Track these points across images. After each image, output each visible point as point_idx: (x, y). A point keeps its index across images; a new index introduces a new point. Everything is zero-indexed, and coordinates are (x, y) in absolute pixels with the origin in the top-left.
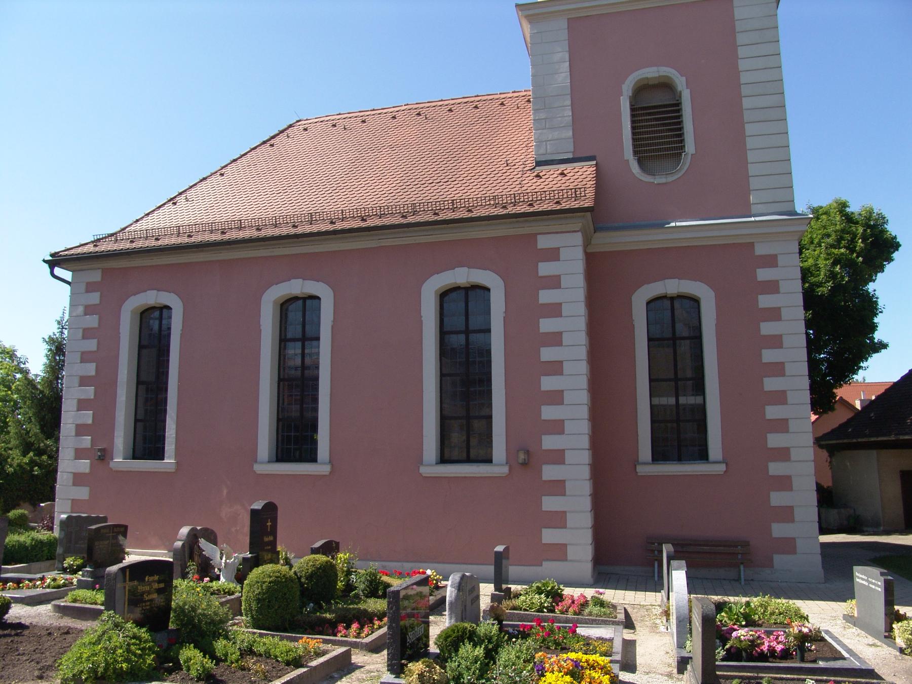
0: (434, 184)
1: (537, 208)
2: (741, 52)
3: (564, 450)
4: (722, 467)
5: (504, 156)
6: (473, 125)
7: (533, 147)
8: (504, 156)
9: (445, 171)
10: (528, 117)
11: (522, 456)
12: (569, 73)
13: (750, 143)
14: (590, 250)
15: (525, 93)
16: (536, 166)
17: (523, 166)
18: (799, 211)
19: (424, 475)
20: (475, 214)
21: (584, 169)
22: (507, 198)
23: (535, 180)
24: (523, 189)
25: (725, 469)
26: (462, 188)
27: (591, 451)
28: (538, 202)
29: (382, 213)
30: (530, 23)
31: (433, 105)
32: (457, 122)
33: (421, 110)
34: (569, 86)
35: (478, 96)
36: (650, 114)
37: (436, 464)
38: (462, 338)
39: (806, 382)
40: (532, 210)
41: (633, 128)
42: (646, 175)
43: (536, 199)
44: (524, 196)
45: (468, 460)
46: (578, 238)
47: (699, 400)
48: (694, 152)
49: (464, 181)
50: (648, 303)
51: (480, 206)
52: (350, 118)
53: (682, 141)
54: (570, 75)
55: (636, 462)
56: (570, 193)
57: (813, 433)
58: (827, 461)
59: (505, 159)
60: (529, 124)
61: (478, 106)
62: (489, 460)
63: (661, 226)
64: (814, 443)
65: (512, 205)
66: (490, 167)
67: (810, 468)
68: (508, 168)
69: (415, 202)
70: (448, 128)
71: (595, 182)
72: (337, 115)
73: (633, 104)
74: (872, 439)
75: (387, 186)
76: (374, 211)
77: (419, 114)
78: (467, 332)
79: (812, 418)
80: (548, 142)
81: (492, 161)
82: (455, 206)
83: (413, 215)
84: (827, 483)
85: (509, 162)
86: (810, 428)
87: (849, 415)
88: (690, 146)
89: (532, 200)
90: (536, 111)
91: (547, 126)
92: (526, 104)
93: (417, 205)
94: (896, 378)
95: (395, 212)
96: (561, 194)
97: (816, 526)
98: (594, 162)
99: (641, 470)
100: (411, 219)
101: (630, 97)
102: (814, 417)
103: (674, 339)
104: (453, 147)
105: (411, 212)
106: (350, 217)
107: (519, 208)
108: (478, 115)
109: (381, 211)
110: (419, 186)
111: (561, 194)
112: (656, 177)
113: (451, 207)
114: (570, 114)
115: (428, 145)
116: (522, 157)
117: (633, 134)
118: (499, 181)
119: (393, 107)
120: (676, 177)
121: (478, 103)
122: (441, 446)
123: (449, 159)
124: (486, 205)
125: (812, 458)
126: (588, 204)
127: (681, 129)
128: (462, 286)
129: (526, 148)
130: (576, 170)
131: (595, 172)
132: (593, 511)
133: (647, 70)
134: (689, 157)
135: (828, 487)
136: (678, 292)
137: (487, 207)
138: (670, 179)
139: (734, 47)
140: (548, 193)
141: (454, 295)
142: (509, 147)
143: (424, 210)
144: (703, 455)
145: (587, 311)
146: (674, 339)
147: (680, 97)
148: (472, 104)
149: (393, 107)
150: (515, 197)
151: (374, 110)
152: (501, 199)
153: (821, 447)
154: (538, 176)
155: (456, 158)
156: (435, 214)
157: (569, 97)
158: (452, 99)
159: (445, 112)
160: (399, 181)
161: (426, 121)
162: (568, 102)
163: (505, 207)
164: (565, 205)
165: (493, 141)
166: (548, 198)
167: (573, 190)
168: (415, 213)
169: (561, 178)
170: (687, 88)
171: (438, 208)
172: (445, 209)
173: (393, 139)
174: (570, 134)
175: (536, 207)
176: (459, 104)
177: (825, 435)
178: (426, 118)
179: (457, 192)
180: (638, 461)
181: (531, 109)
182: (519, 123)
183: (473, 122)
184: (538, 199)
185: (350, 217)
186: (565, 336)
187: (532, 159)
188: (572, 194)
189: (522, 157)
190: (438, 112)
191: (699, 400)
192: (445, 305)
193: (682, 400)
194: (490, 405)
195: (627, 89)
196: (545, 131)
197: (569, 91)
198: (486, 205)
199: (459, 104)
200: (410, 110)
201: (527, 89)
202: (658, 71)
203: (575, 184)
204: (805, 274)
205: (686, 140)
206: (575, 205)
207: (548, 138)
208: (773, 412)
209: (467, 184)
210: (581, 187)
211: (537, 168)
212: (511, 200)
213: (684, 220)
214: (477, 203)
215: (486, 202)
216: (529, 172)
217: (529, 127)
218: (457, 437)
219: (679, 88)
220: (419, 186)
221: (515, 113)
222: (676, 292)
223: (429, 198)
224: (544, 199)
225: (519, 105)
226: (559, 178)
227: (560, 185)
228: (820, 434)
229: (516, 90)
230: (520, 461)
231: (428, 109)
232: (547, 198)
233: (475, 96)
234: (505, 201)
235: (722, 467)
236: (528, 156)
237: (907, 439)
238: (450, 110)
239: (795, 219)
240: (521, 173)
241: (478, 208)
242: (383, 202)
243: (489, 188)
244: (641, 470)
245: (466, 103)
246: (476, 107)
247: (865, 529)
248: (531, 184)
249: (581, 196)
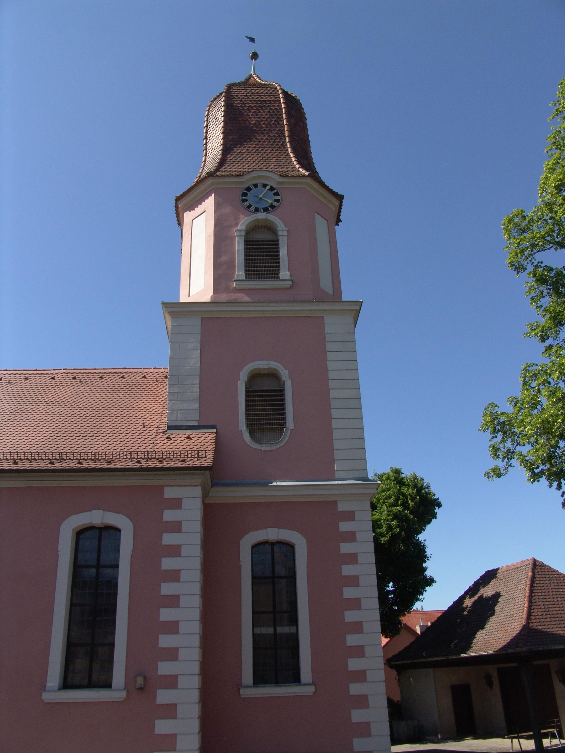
0: (81, 437)
1: (166, 464)
2: (330, 356)
3: (177, 676)
4: (312, 689)
5: (142, 419)
6: (119, 392)
7: (167, 414)
8: (142, 419)
9: (91, 427)
10: (164, 390)
11: (140, 681)
12: (199, 359)
13: (335, 424)
14: (207, 501)
15: (163, 370)
16: (168, 430)
17: (157, 429)
18: (371, 478)
19: (46, 701)
20: (114, 465)
21: (207, 435)
22: (141, 454)
23: (166, 441)
24: (156, 447)
25: (314, 690)
26: (105, 443)
27: (201, 676)
28: (167, 460)
29: (33, 458)
30: (172, 317)
31: (87, 372)
32: (105, 387)
33: (77, 374)
34: (199, 368)
35: (125, 369)
36: (261, 396)
37: (59, 689)
38: (93, 571)
39: (376, 615)
40: (161, 465)
41: (247, 406)
42: (255, 444)
43: (165, 457)
44: (155, 454)
45: (90, 685)
46: (198, 492)
47: (293, 630)
48: (293, 428)
49: (107, 437)
50: (253, 547)
51: (118, 459)
52: (15, 374)
53: (284, 419)
54: (200, 360)
55: (240, 685)
56: (193, 454)
57: (384, 656)
58: (396, 679)
59: (143, 422)
60: (165, 395)
61: (125, 376)
62: (108, 685)
63: (265, 484)
64: (385, 664)
65: (145, 460)
66: (130, 427)
67: (382, 688)
68: (144, 429)
69: (63, 451)
70: (98, 391)
71: (214, 446)
72: (4, 370)
73: (248, 387)
74: (429, 659)
75: (40, 435)
76: (26, 455)
77: (75, 378)
78: (98, 566)
79: (383, 642)
80: (179, 411)
81: (132, 422)
82: (97, 457)
83: (60, 462)
84: (397, 698)
85: (145, 424)
86: (381, 653)
87: (412, 639)
88: (290, 423)
89: (162, 458)
90: (171, 385)
91: (179, 399)
92: (164, 379)
93: (64, 453)
94: (446, 608)
95: (44, 458)
96: (186, 454)
97: (389, 739)
98: (215, 430)
99: (245, 693)
100: (58, 466)
101: (246, 381)
102: (385, 641)
103: (274, 578)
104: (101, 408)
105: (58, 460)
106: (3, 459)
107: (150, 463)
108: (124, 383)
109: (32, 456)
110: (68, 437)
111: (186, 454)
112: (263, 445)
113: (93, 458)
114: (198, 390)
115: (79, 404)
116: (157, 421)
117: (247, 410)
118: (136, 439)
119: (54, 370)
120: (278, 446)
121: (125, 374)
122: (65, 672)
123: (96, 417)
124: (123, 459)
125: (384, 679)
126: (208, 463)
127: (284, 409)
128: (97, 526)
129: (161, 414)
130: (200, 435)
131: (215, 438)
132: (200, 733)
133: (260, 362)
134: (289, 431)
135: (398, 701)
136: (277, 539)
137: (124, 460)
138: (274, 448)
139: (324, 352)
140: (175, 452)
141: (89, 534)
142: (147, 412)
143: (70, 459)
144: (296, 679)
145: (202, 552)
146: (274, 578)
147: (284, 385)
148: (119, 374)
149: (54, 370)
150: (148, 454)
151: (36, 370)
152: (136, 455)
153: (391, 667)
154: (168, 438)
155: (102, 417)
156: (79, 463)
157: (198, 377)
158: (104, 369)
159: (97, 378)
160: (50, 432)
161: (80, 384)
162: (197, 381)
163: (139, 462)
164: (189, 464)
165: (134, 406)
166: (175, 456)
167: (196, 452)
168: (61, 460)
169: (187, 441)
170: (289, 379)
171: (82, 458)
172: (88, 459)
173: (50, 396)
174: (197, 406)
175: (165, 463)
176: (109, 373)
177: (394, 657)
178: (80, 382)
179: (100, 445)
180: (241, 685)
181: (167, 383)
182: (157, 393)
183: (119, 389)
184: (167, 456)
185: (3, 459)
186: (182, 573)
187: (165, 423)
188: (195, 455)
189: (157, 421)
190: (91, 378)
191: (293, 630)
192: (81, 543)
193: (279, 630)
194: (113, 633)
195: (244, 375)
196: (177, 402)
197: (198, 373)
198: (123, 459)
199: (109, 373)
200: (67, 373)
201: (165, 367)
202: (268, 364)
203: (199, 446)
204: (376, 524)
205: (287, 418)
206: (197, 464)
207: (179, 408)
208: (352, 640)
209: (109, 440)
210: (203, 449)
211: (168, 431)
212: (145, 456)
213: (284, 480)
214: (116, 456)
215: (123, 456)
216: (161, 434)
217: (165, 397)
218: (81, 663)
219: (284, 378)
220: (68, 437)
221: (154, 385)
222: (276, 538)
223: (75, 448)
224: (172, 457)
225: (158, 379)
226: (186, 441)
227: (186, 447)
228: (389, 656)
229: (157, 367)
230: (138, 686)
231: (83, 374)
232: (175, 456)
233: (123, 369)
234: (139, 457)
235: (312, 689)
236: (162, 421)
237: (454, 659)
238: (101, 378)
239: (365, 484)
240: (155, 434)
241: (116, 460)
242: (34, 449)
243: (127, 445)
244: (245, 693)
245: (115, 373)
246: (123, 377)
247: (428, 738)
248: (162, 444)
249: (202, 457)
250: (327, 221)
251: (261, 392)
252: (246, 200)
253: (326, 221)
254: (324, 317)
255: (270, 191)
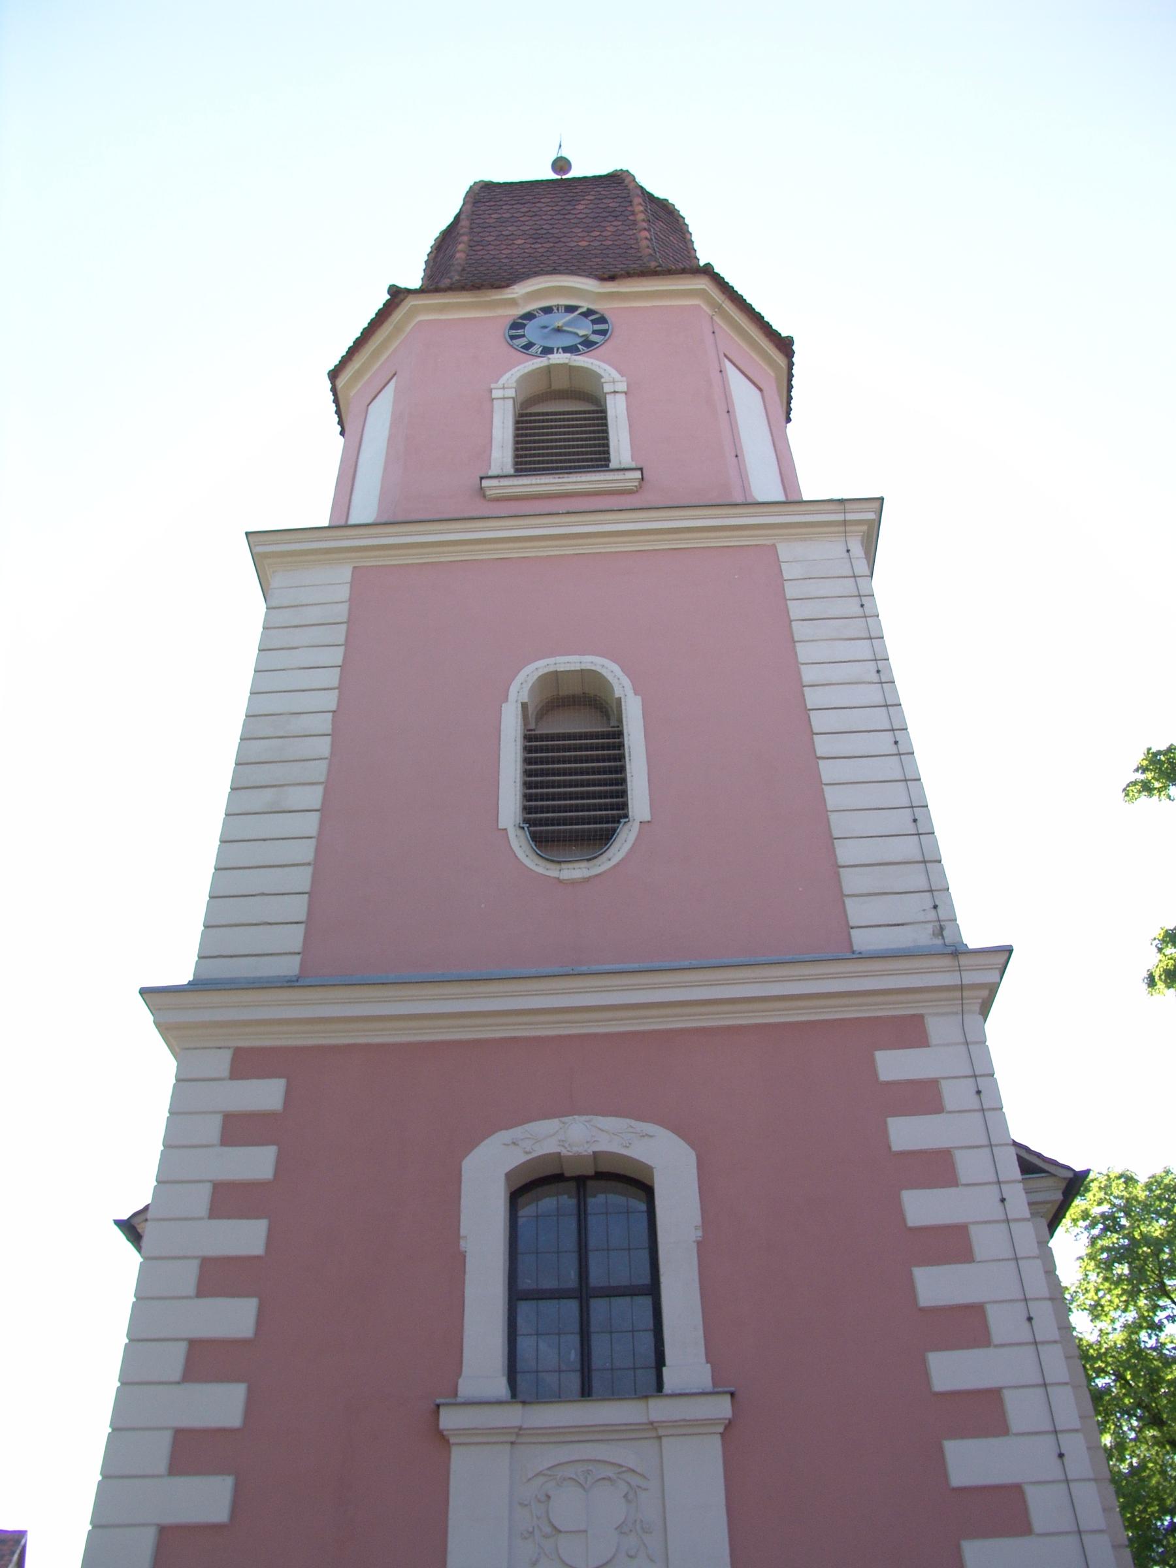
48: (647, 817)
202: (570, 359)
205: (629, 779)
250: (760, 390)
251: (557, 446)
252: (523, 336)
253: (757, 392)
254: (921, 1017)
255: (583, 317)
